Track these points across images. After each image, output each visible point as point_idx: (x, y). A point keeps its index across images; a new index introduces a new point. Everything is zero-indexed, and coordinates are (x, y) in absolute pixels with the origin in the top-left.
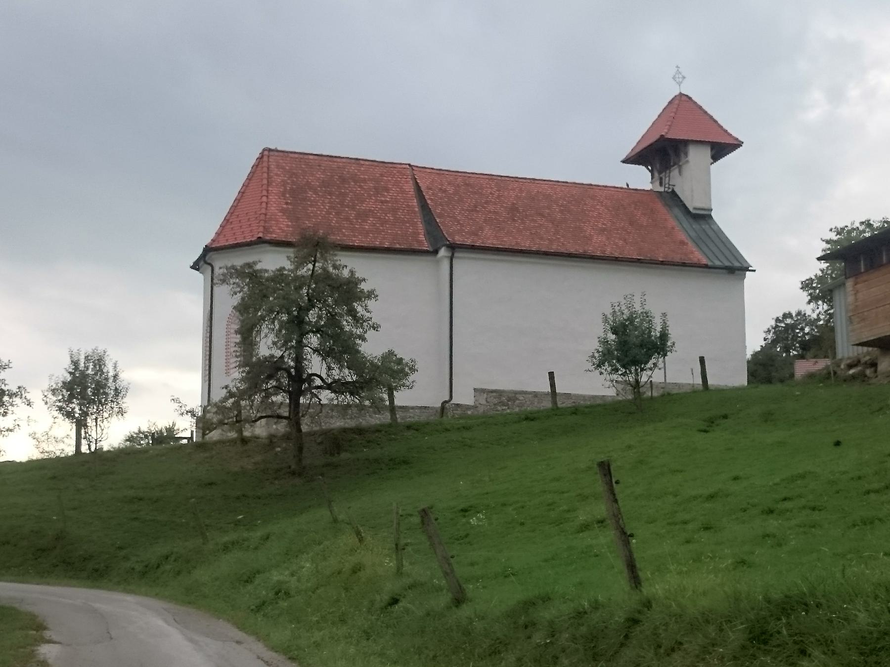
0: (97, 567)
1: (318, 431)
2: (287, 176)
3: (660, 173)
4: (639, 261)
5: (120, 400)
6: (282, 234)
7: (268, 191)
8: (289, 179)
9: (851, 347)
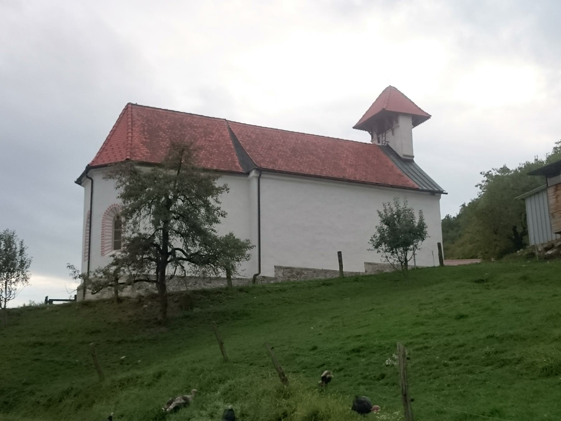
0: (7, 400)
1: (184, 292)
2: (145, 121)
3: (378, 134)
4: (377, 184)
5: (24, 269)
6: (143, 157)
7: (132, 130)
8: (146, 123)
9: (555, 234)
